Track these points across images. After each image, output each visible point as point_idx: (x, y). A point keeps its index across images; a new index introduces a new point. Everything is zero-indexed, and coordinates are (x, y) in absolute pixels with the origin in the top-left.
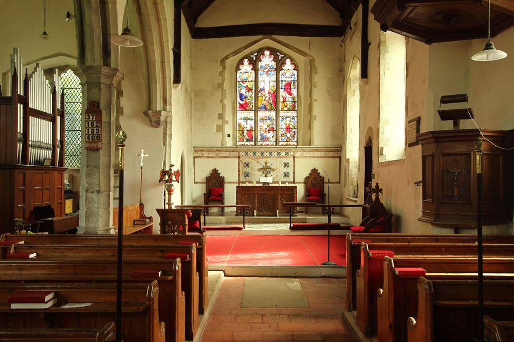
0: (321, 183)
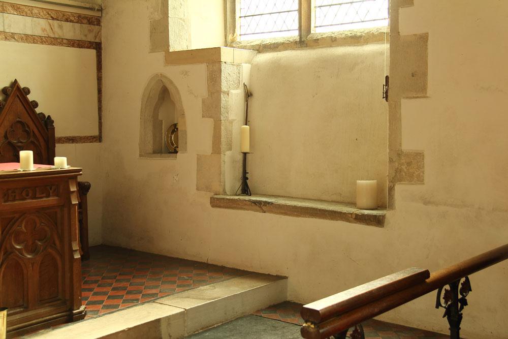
0: (42, 143)
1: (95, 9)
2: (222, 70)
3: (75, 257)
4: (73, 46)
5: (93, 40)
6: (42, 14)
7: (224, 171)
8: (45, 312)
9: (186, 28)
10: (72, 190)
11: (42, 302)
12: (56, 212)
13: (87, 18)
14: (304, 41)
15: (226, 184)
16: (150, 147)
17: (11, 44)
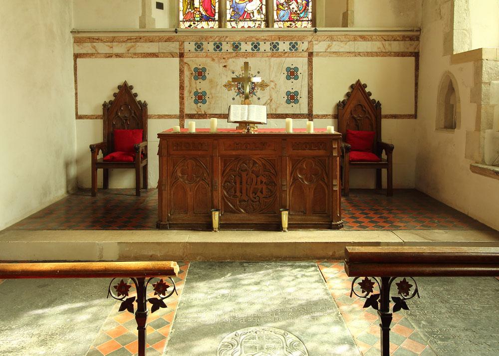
0: (373, 118)
1: (414, 30)
2: (484, 65)
3: (334, 189)
4: (398, 56)
5: (413, 51)
6: (378, 38)
7: (484, 145)
8: (315, 219)
9: (468, 36)
10: (334, 147)
11: (315, 213)
12: (326, 160)
13: (409, 37)
14: (176, 31)
15: (486, 156)
16: (442, 124)
17: (359, 59)
